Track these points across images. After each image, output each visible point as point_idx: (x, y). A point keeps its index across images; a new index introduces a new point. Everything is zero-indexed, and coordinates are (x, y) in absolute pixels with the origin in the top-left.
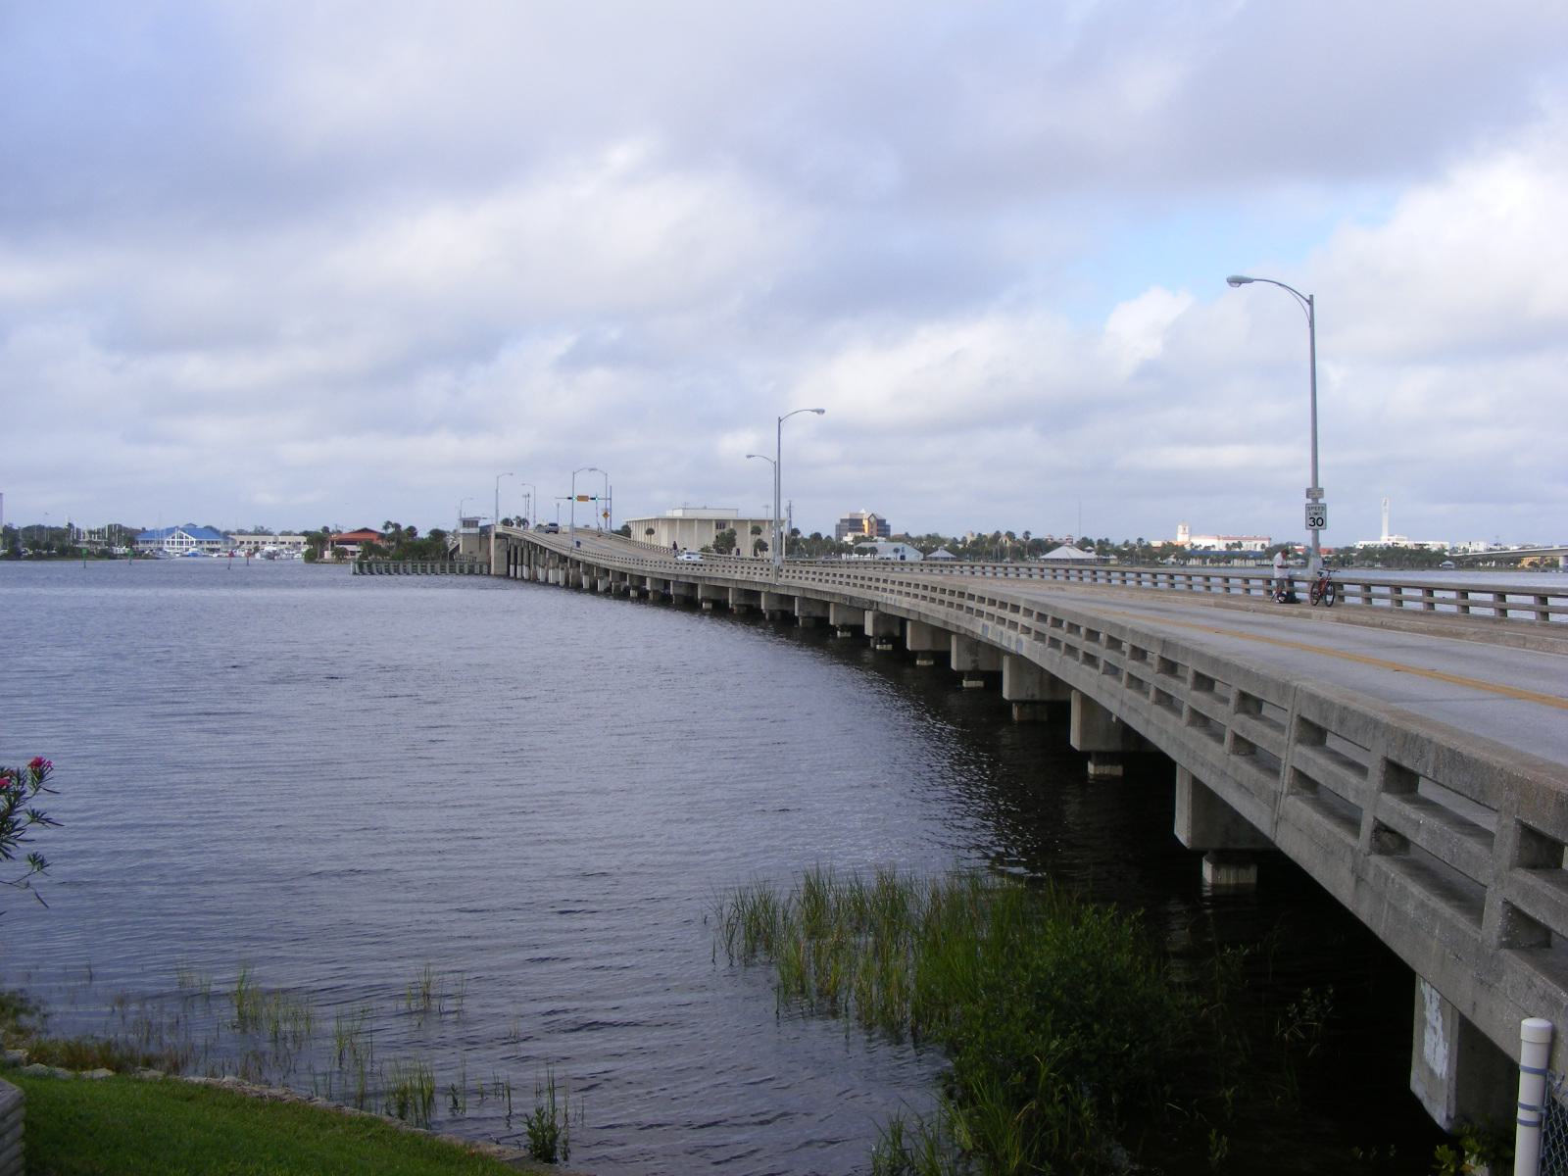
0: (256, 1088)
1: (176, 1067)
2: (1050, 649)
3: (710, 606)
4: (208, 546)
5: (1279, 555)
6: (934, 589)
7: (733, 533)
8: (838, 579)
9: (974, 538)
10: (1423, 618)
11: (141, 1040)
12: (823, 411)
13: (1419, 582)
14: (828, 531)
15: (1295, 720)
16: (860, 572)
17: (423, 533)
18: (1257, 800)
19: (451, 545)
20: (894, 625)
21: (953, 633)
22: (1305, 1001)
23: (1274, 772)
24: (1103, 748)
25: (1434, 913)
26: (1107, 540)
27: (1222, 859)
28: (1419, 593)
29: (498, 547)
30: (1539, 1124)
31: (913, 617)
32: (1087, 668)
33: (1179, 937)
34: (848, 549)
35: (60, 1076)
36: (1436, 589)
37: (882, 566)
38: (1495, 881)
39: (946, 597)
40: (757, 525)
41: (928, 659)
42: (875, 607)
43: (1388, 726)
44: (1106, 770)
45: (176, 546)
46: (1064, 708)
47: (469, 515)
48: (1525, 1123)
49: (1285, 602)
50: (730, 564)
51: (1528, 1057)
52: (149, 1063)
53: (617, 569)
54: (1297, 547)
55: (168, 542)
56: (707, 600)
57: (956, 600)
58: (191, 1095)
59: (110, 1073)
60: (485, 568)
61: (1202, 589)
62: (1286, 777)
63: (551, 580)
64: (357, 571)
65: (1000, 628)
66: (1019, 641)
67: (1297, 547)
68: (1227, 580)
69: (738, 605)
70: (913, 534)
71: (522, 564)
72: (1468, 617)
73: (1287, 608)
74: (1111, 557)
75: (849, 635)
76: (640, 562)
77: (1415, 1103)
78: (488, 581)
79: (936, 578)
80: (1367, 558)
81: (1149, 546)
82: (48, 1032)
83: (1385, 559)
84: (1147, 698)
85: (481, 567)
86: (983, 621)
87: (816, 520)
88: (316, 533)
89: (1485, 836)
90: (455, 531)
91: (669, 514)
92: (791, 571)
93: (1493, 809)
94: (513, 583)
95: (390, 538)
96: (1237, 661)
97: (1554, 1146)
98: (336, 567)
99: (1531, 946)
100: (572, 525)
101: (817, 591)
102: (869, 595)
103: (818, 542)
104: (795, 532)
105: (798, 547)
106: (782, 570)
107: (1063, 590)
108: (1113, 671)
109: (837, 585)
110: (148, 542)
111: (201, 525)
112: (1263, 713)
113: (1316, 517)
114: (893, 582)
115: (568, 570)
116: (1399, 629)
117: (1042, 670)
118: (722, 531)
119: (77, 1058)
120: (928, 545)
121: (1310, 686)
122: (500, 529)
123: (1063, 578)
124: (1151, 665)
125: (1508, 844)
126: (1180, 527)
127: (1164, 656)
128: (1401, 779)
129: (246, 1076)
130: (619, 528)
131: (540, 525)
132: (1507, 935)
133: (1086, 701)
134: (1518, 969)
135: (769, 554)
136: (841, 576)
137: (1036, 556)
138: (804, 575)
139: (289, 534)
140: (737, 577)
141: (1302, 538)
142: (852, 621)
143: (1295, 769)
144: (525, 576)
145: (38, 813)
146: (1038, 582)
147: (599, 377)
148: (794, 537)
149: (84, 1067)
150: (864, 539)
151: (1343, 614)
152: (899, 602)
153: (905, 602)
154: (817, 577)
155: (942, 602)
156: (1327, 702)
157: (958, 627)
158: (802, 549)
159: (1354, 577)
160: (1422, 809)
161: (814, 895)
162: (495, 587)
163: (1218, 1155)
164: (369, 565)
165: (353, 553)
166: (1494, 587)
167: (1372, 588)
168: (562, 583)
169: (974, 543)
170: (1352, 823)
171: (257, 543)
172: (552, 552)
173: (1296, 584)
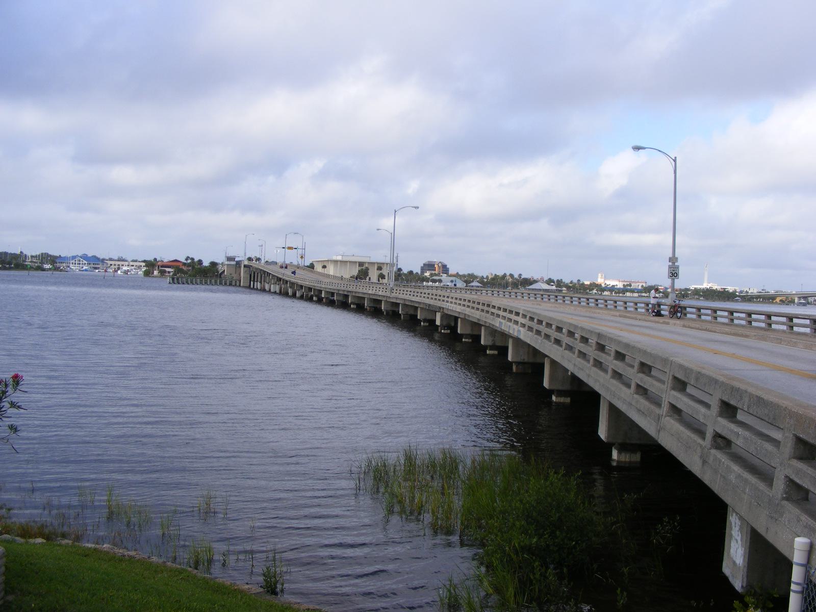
0: (121, 551)
1: (78, 538)
2: (536, 336)
3: (355, 306)
4: (93, 266)
5: (653, 292)
6: (474, 302)
7: (367, 269)
8: (423, 295)
9: (493, 276)
10: (727, 327)
11: (59, 525)
12: (418, 208)
13: (727, 308)
14: (417, 270)
15: (671, 378)
16: (434, 292)
17: (206, 263)
18: (649, 418)
19: (220, 269)
20: (451, 321)
21: (483, 325)
22: (665, 524)
23: (658, 404)
24: (561, 388)
25: (746, 480)
26: (561, 280)
27: (623, 448)
28: (726, 314)
29: (245, 272)
30: (802, 592)
31: (462, 316)
32: (555, 346)
33: (599, 489)
34: (427, 280)
35: (18, 542)
36: (718, 310)
37: (445, 289)
38: (781, 465)
39: (480, 307)
40: (379, 265)
41: (469, 339)
42: (442, 310)
43: (723, 383)
44: (562, 400)
45: (76, 265)
46: (542, 366)
47: (231, 254)
48: (795, 592)
49: (656, 315)
50: (366, 285)
51: (798, 557)
52: (64, 536)
53: (307, 286)
54: (660, 287)
55: (73, 263)
56: (354, 304)
57: (486, 308)
58: (87, 553)
59: (45, 541)
60: (238, 282)
61: (612, 307)
62: (665, 407)
63: (272, 290)
64: (171, 282)
65: (509, 324)
66: (519, 331)
67: (660, 287)
68: (625, 303)
69: (370, 307)
70: (461, 273)
71: (257, 282)
72: (751, 327)
73: (657, 319)
74: (563, 289)
75: (427, 324)
76: (319, 282)
77: (725, 579)
78: (240, 289)
79: (473, 297)
80: (696, 294)
81: (583, 284)
82: (10, 518)
83: (705, 295)
84: (589, 363)
85: (236, 282)
86: (500, 320)
87: (411, 263)
88: (150, 261)
89: (776, 443)
90: (222, 263)
91: (335, 258)
92: (398, 290)
93: (780, 428)
94: (253, 291)
95: (189, 265)
96: (639, 346)
97: (810, 604)
98: (160, 279)
99: (798, 500)
100: (284, 262)
101: (411, 301)
102: (439, 304)
103: (412, 276)
104: (400, 270)
105: (400, 277)
106: (393, 289)
107: (540, 305)
108: (570, 348)
109: (422, 298)
110: (62, 263)
111: (90, 255)
112: (652, 373)
113: (674, 272)
114: (452, 298)
115: (281, 285)
116: (715, 332)
117: (529, 345)
118: (362, 268)
119: (26, 533)
120: (468, 279)
121: (680, 360)
122: (246, 263)
123: (540, 299)
124: (591, 346)
125: (788, 447)
126: (600, 275)
127: (599, 342)
128: (728, 410)
129: (115, 544)
130: (308, 264)
131: (267, 261)
132: (786, 494)
133: (553, 363)
134: (792, 511)
135: (385, 281)
136: (425, 293)
137: (524, 287)
138: (405, 292)
139: (136, 261)
140: (370, 292)
141: (664, 282)
142: (430, 317)
143: (670, 403)
144: (259, 287)
145: (14, 403)
146: (526, 300)
147: (334, 188)
148: (399, 272)
149: (30, 537)
150: (436, 275)
151: (686, 323)
152: (455, 308)
153: (459, 309)
154: (412, 293)
155: (478, 309)
156: (689, 369)
157: (485, 322)
158: (403, 279)
159: (692, 304)
160: (740, 426)
161: (410, 459)
162: (243, 293)
163: (622, 601)
164: (178, 279)
165: (169, 272)
166: (765, 312)
167: (718, 311)
168: (278, 291)
169: (493, 279)
170: (701, 433)
171: (119, 265)
172: (273, 276)
173: (662, 307)
